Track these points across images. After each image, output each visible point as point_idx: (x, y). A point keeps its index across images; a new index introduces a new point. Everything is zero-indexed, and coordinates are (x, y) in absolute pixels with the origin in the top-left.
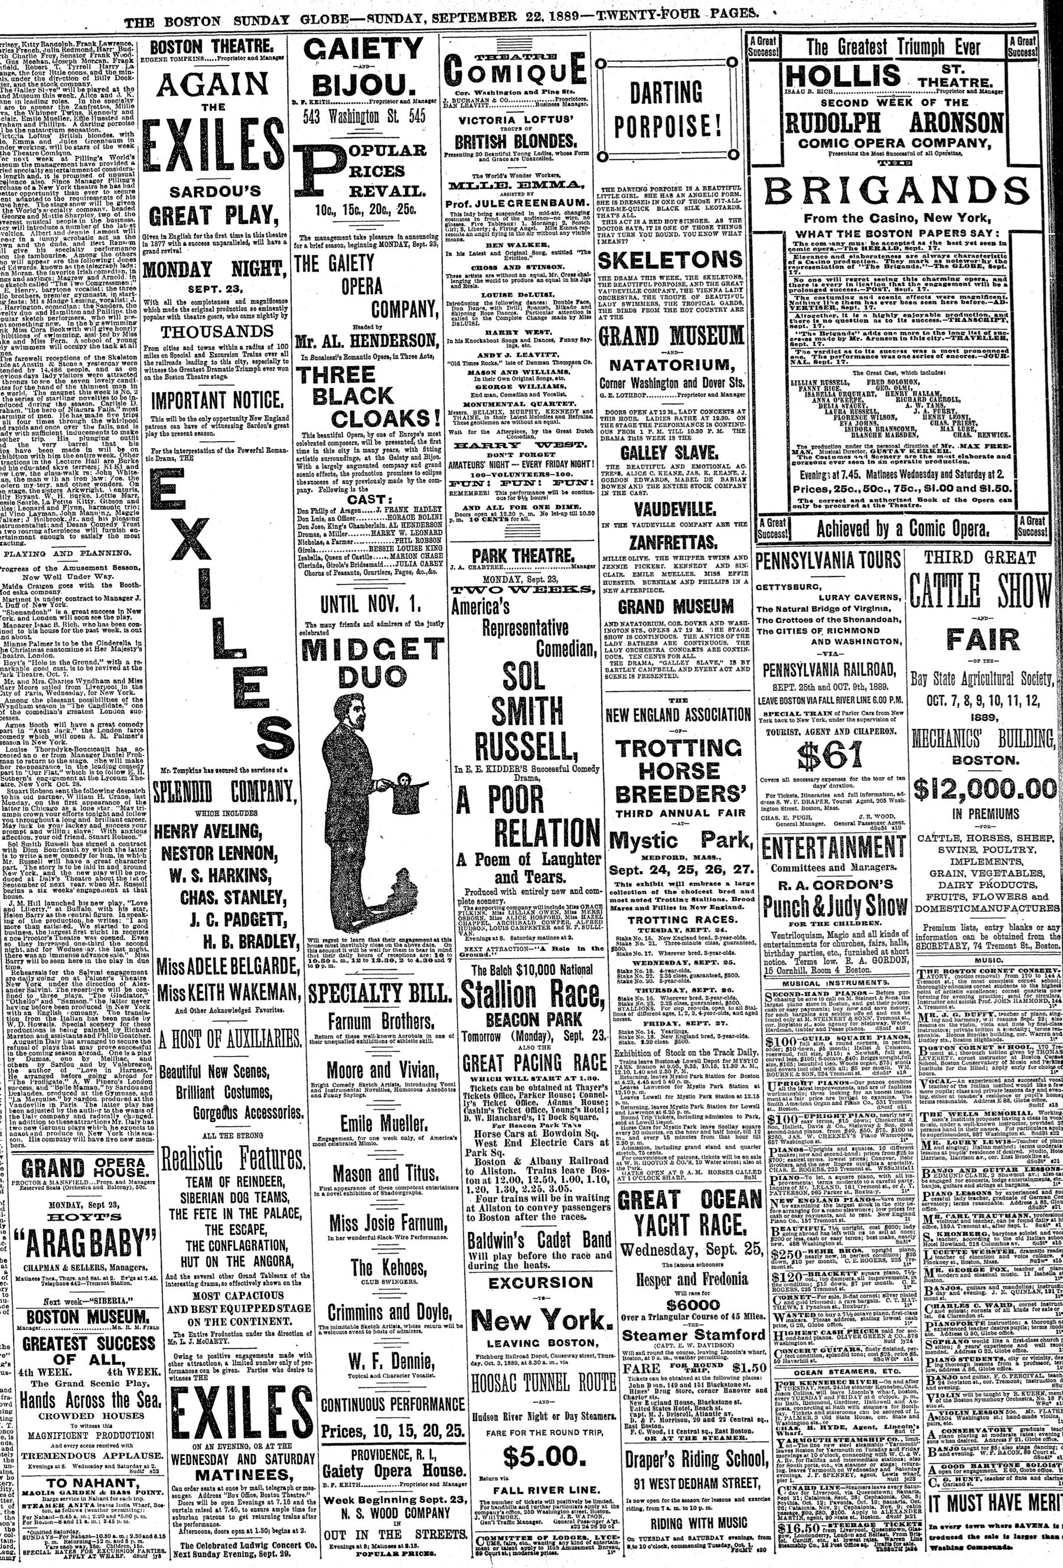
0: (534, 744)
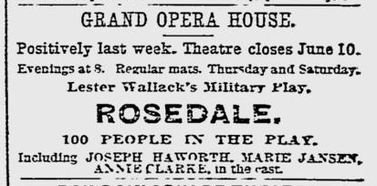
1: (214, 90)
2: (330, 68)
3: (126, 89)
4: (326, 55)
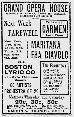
0: (64, 8)
1: (18, 48)
2: (32, 97)
3: (13, 77)
4: (27, 99)
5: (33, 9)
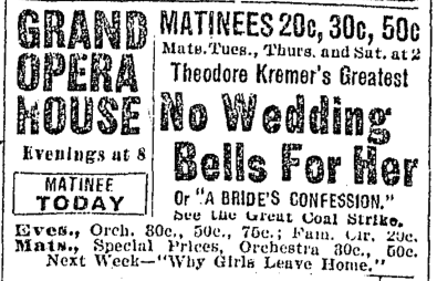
5: (60, 85)
